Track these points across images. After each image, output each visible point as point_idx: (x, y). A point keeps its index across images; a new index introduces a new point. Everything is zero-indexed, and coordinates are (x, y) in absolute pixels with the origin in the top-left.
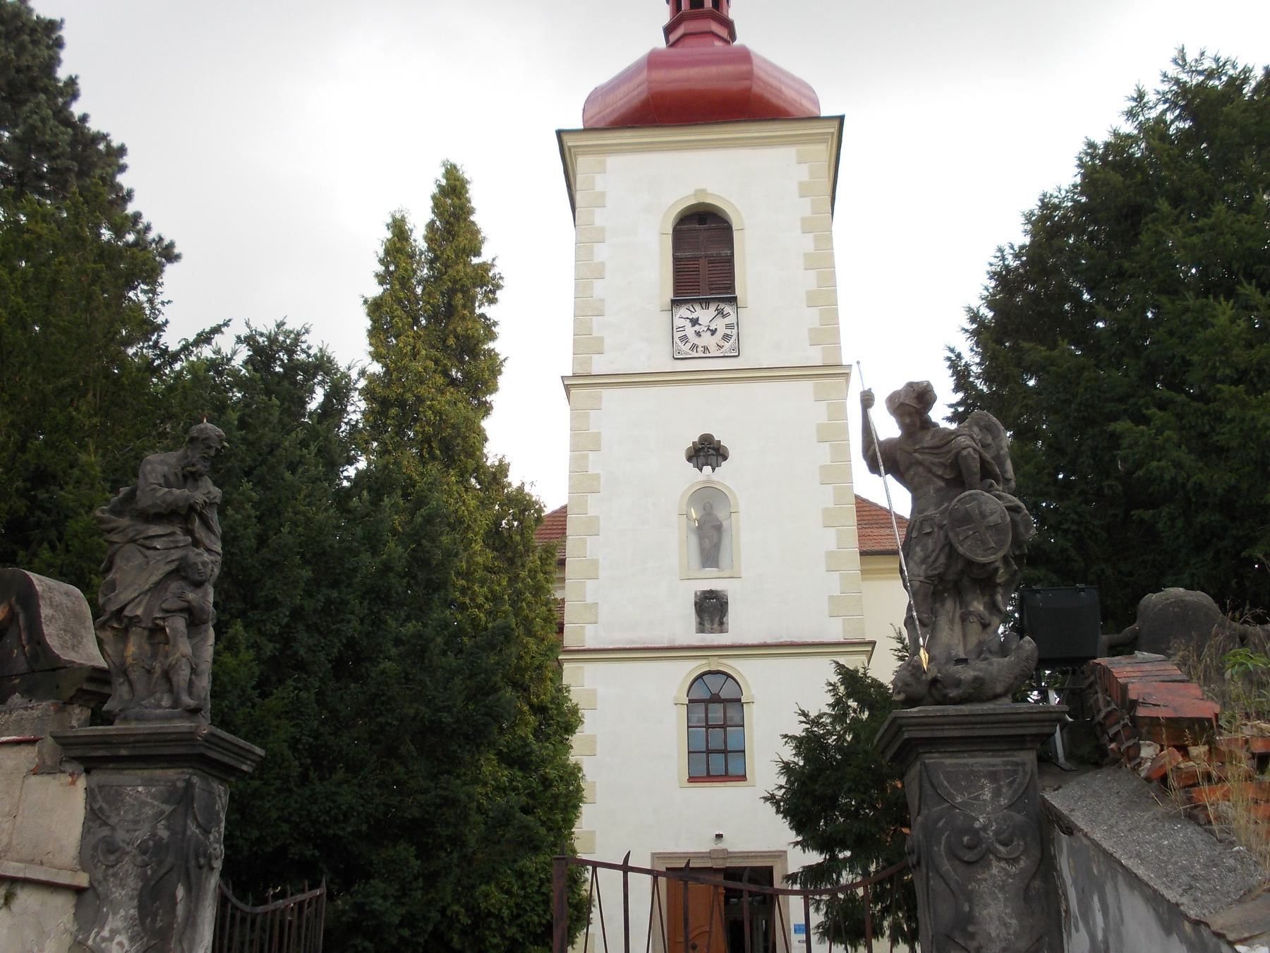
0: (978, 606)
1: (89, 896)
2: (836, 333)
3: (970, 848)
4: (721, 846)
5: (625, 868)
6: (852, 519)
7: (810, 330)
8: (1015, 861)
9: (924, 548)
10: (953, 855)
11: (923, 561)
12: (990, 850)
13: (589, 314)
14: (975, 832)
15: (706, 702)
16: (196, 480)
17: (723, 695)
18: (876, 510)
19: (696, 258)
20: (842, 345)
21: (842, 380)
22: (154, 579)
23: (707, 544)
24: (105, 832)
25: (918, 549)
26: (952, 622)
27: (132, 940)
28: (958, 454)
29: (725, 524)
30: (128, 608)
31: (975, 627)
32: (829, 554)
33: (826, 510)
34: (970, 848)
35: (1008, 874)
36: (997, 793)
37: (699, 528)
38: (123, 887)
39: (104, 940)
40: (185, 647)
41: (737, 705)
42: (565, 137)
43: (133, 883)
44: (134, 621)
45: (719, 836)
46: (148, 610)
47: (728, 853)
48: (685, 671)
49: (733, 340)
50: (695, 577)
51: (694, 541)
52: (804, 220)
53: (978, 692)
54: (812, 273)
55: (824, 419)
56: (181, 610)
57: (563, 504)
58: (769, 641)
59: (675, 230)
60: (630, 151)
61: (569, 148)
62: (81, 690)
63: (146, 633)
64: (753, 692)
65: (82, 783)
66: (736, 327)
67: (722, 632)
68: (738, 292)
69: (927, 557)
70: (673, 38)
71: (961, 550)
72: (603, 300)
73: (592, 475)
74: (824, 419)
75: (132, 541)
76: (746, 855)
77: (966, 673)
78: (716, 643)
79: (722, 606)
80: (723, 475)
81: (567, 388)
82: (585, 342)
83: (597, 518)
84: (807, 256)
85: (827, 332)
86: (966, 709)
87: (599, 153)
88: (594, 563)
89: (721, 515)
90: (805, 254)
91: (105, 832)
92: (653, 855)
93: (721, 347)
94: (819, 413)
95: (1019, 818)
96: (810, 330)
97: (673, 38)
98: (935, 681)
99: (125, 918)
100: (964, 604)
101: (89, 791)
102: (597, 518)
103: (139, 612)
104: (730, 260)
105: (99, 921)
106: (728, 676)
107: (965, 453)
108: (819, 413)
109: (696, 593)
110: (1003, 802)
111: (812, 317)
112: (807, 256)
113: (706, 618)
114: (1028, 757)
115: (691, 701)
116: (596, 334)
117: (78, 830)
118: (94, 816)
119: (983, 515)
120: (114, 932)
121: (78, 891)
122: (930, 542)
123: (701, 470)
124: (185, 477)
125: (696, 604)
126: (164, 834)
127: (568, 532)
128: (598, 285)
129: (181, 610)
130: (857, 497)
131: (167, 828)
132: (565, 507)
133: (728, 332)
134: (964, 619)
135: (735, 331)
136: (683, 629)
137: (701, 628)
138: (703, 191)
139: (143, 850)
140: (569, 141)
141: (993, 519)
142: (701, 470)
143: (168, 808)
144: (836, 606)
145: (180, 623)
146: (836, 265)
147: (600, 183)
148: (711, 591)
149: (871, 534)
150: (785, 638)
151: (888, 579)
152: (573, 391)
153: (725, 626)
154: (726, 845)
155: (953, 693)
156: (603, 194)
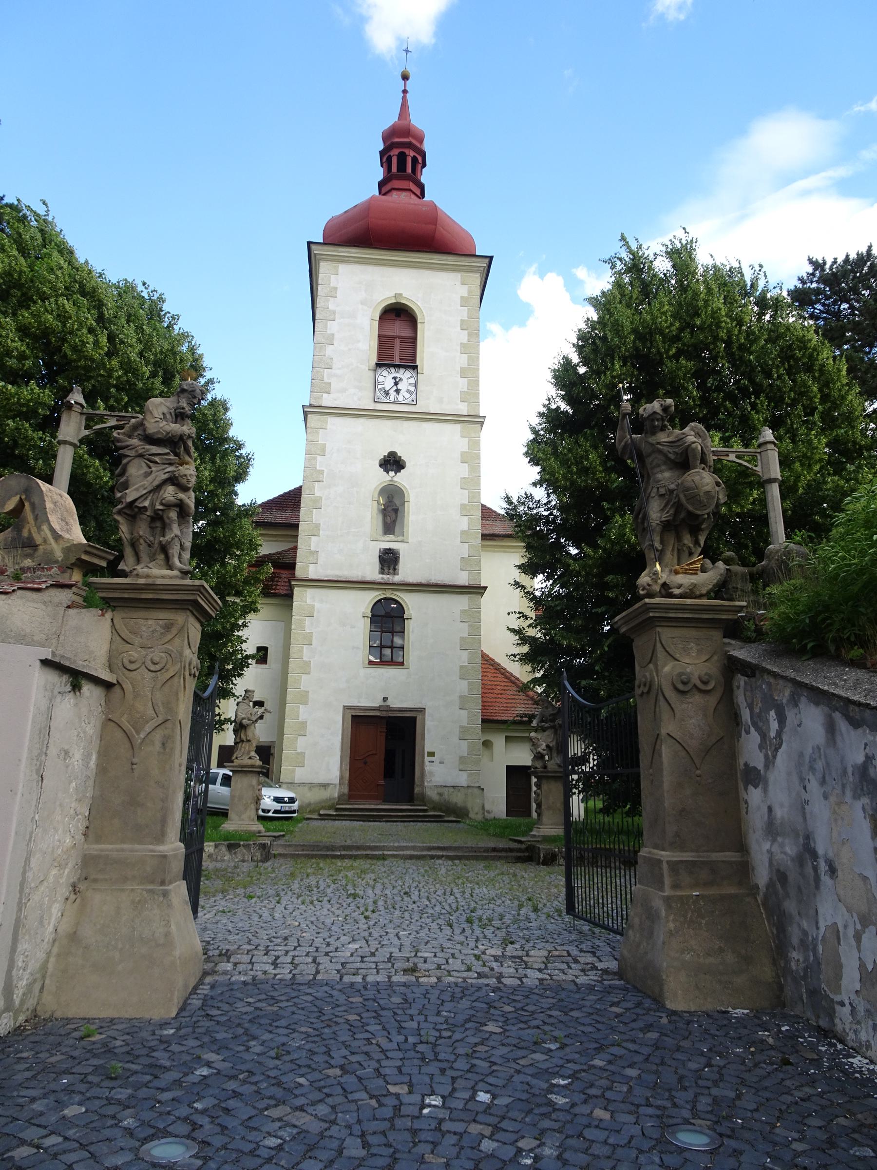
1: (117, 689)
2: (477, 395)
4: (386, 703)
6: (479, 513)
16: (183, 419)
21: (478, 426)
23: (389, 520)
28: (689, 445)
30: (139, 501)
32: (463, 532)
33: (462, 505)
37: (384, 510)
41: (401, 619)
42: (313, 247)
46: (152, 504)
48: (370, 598)
51: (380, 518)
52: (462, 321)
55: (465, 449)
57: (297, 486)
62: (79, 559)
63: (149, 519)
68: (418, 363)
70: (383, 191)
74: (466, 449)
75: (141, 456)
76: (401, 710)
80: (401, 479)
81: (306, 414)
82: (318, 385)
83: (321, 498)
85: (472, 394)
88: (318, 526)
89: (397, 502)
92: (344, 706)
94: (463, 445)
96: (461, 697)
97: (384, 190)
103: (146, 504)
107: (694, 446)
108: (463, 445)
111: (463, 384)
116: (326, 380)
124: (176, 416)
125: (380, 556)
127: (302, 505)
129: (175, 505)
130: (483, 506)
132: (301, 487)
136: (371, 571)
137: (382, 571)
140: (316, 250)
144: (467, 563)
145: (173, 515)
146: (481, 353)
147: (334, 281)
148: (390, 549)
151: (494, 551)
152: (310, 416)
154: (389, 703)
155: (677, 591)
156: (336, 289)
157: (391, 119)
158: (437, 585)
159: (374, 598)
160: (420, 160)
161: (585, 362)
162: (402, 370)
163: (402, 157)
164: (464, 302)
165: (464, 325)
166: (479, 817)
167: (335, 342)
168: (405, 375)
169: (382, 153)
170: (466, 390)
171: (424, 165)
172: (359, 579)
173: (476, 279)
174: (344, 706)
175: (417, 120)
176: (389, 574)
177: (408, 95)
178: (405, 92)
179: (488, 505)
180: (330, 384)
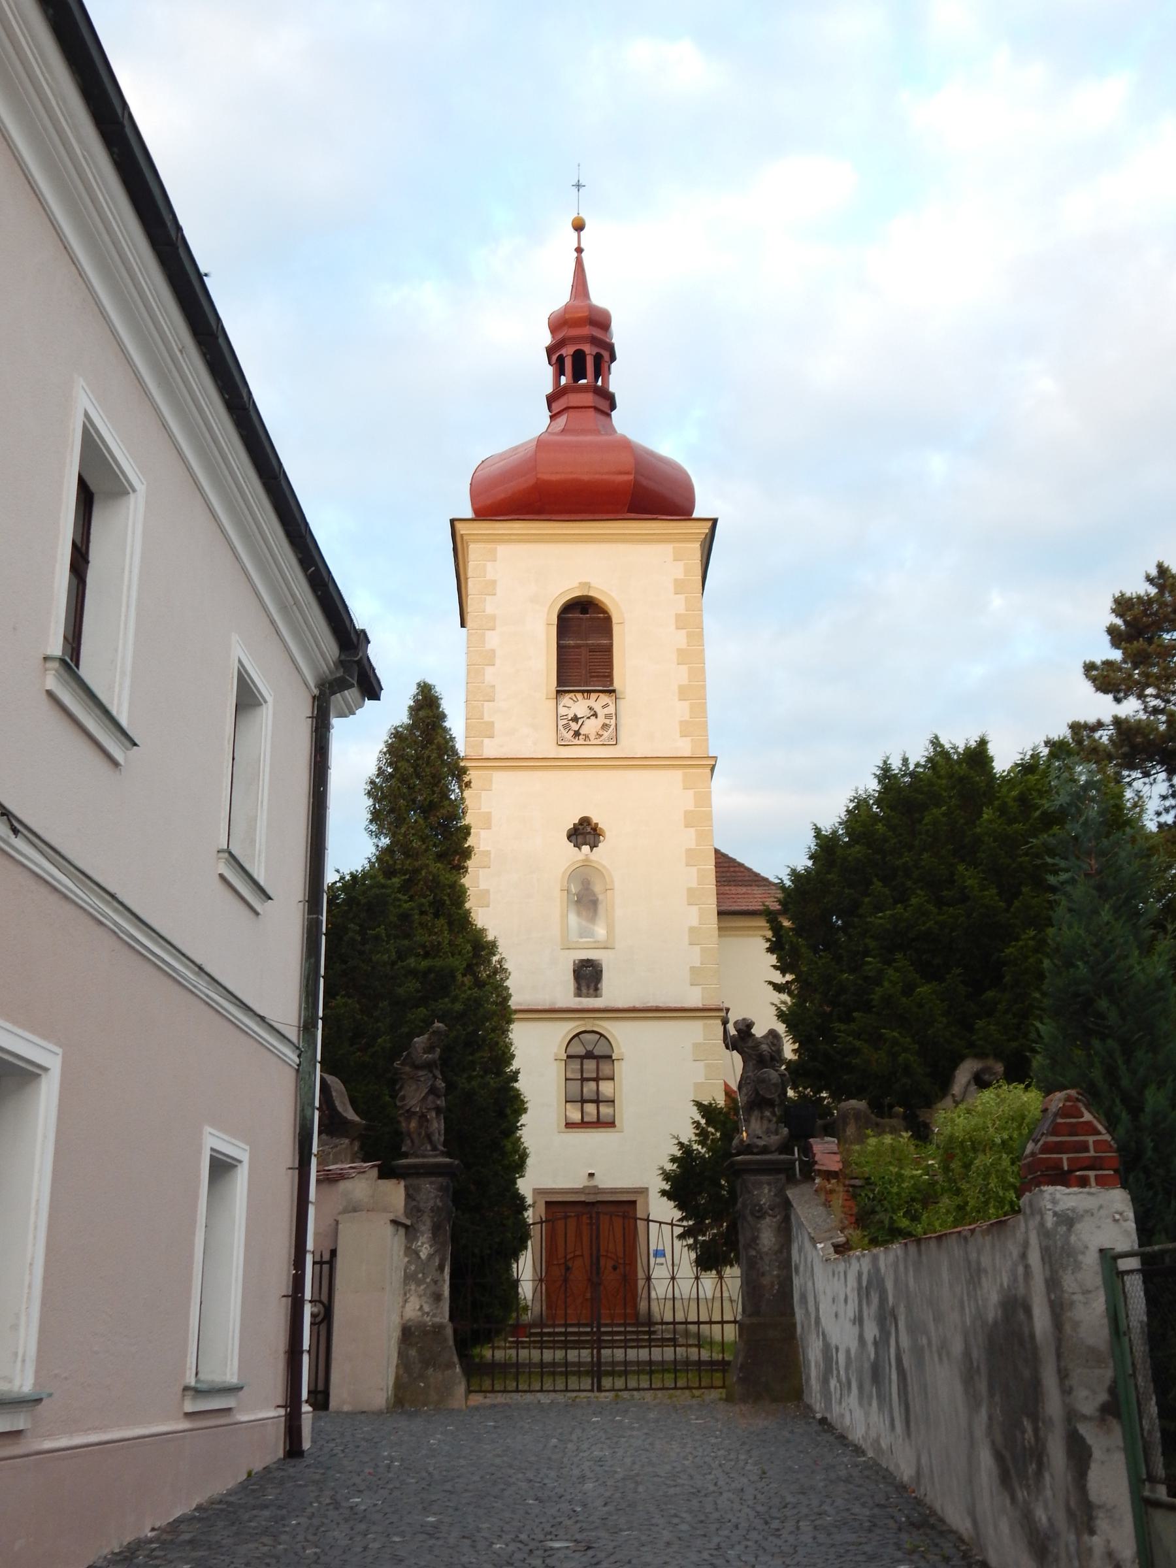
0: (768, 1114)
3: (759, 1211)
5: (672, 1224)
6: (710, 866)
7: (681, 722)
8: (775, 1216)
9: (747, 1089)
10: (752, 1214)
11: (746, 1095)
12: (765, 1212)
13: (481, 699)
14: (761, 1206)
15: (582, 1058)
17: (596, 1053)
18: (735, 867)
19: (578, 646)
20: (712, 789)
22: (423, 1095)
24: (414, 1203)
25: (744, 1089)
26: (756, 1120)
27: (431, 1246)
29: (601, 897)
31: (765, 1122)
32: (692, 930)
34: (759, 1211)
35: (772, 1222)
36: (770, 1191)
38: (425, 1225)
39: (419, 1246)
40: (435, 1125)
42: (458, 525)
43: (429, 1223)
44: (415, 1113)
45: (591, 1175)
47: (599, 1189)
49: (612, 731)
50: (574, 947)
52: (678, 616)
53: (765, 1150)
54: (684, 668)
55: (690, 806)
56: (434, 1109)
58: (638, 1005)
59: (559, 617)
60: (520, 541)
61: (462, 535)
64: (623, 1050)
65: (402, 1183)
66: (614, 717)
67: (596, 996)
68: (617, 684)
69: (748, 1093)
71: (761, 1093)
72: (493, 686)
73: (484, 851)
74: (690, 806)
75: (412, 1078)
76: (614, 1191)
77: (761, 1143)
78: (591, 1006)
79: (597, 973)
80: (601, 855)
84: (680, 651)
85: (695, 726)
86: (759, 1157)
87: (493, 541)
89: (597, 888)
90: (678, 650)
91: (414, 1203)
92: (534, 1190)
93: (601, 736)
94: (687, 800)
95: (778, 1200)
96: (681, 722)
97: (557, 406)
98: (749, 1145)
99: (427, 1237)
100: (762, 1113)
101: (406, 1187)
102: (487, 891)
103: (418, 1109)
104: (608, 650)
105: (416, 1239)
106: (601, 1035)
109: (574, 962)
110: (772, 1194)
111: (682, 709)
112: (680, 651)
113: (583, 983)
114: (782, 1177)
115: (568, 1057)
116: (486, 718)
117: (403, 1203)
118: (409, 1197)
119: (770, 1080)
120: (423, 1244)
121: (406, 1227)
122: (749, 1087)
123: (580, 849)
125: (574, 971)
126: (440, 1204)
128: (489, 671)
129: (434, 1109)
130: (717, 851)
131: (441, 1201)
133: (607, 721)
134: (762, 1118)
135: (613, 722)
137: (579, 993)
138: (588, 585)
139: (432, 1210)
140: (461, 528)
141: (774, 1081)
142: (580, 849)
143: (441, 1194)
146: (708, 697)
148: (588, 961)
149: (728, 892)
150: (652, 1003)
151: (749, 936)
153: (599, 992)
155: (755, 1150)
156: (494, 582)
157: (560, 297)
158: (657, 1010)
159: (568, 1033)
160: (605, 354)
161: (848, 834)
162: (594, 696)
163: (579, 357)
164: (680, 587)
165: (681, 622)
166: (731, 1333)
167: (498, 662)
168: (599, 702)
169: (550, 351)
170: (687, 718)
171: (613, 358)
172: (547, 1007)
173: (695, 548)
174: (534, 1190)
175: (599, 297)
176: (588, 996)
177: (583, 255)
178: (579, 250)
179: (723, 850)
180: (493, 723)
